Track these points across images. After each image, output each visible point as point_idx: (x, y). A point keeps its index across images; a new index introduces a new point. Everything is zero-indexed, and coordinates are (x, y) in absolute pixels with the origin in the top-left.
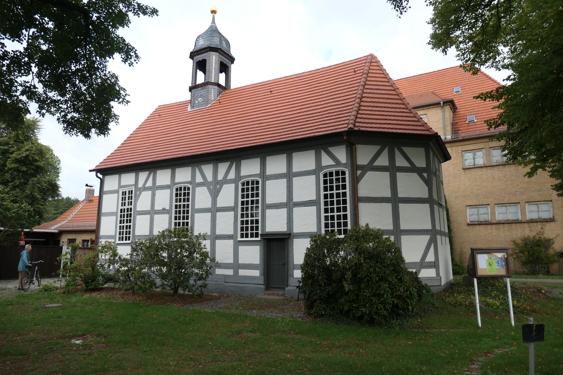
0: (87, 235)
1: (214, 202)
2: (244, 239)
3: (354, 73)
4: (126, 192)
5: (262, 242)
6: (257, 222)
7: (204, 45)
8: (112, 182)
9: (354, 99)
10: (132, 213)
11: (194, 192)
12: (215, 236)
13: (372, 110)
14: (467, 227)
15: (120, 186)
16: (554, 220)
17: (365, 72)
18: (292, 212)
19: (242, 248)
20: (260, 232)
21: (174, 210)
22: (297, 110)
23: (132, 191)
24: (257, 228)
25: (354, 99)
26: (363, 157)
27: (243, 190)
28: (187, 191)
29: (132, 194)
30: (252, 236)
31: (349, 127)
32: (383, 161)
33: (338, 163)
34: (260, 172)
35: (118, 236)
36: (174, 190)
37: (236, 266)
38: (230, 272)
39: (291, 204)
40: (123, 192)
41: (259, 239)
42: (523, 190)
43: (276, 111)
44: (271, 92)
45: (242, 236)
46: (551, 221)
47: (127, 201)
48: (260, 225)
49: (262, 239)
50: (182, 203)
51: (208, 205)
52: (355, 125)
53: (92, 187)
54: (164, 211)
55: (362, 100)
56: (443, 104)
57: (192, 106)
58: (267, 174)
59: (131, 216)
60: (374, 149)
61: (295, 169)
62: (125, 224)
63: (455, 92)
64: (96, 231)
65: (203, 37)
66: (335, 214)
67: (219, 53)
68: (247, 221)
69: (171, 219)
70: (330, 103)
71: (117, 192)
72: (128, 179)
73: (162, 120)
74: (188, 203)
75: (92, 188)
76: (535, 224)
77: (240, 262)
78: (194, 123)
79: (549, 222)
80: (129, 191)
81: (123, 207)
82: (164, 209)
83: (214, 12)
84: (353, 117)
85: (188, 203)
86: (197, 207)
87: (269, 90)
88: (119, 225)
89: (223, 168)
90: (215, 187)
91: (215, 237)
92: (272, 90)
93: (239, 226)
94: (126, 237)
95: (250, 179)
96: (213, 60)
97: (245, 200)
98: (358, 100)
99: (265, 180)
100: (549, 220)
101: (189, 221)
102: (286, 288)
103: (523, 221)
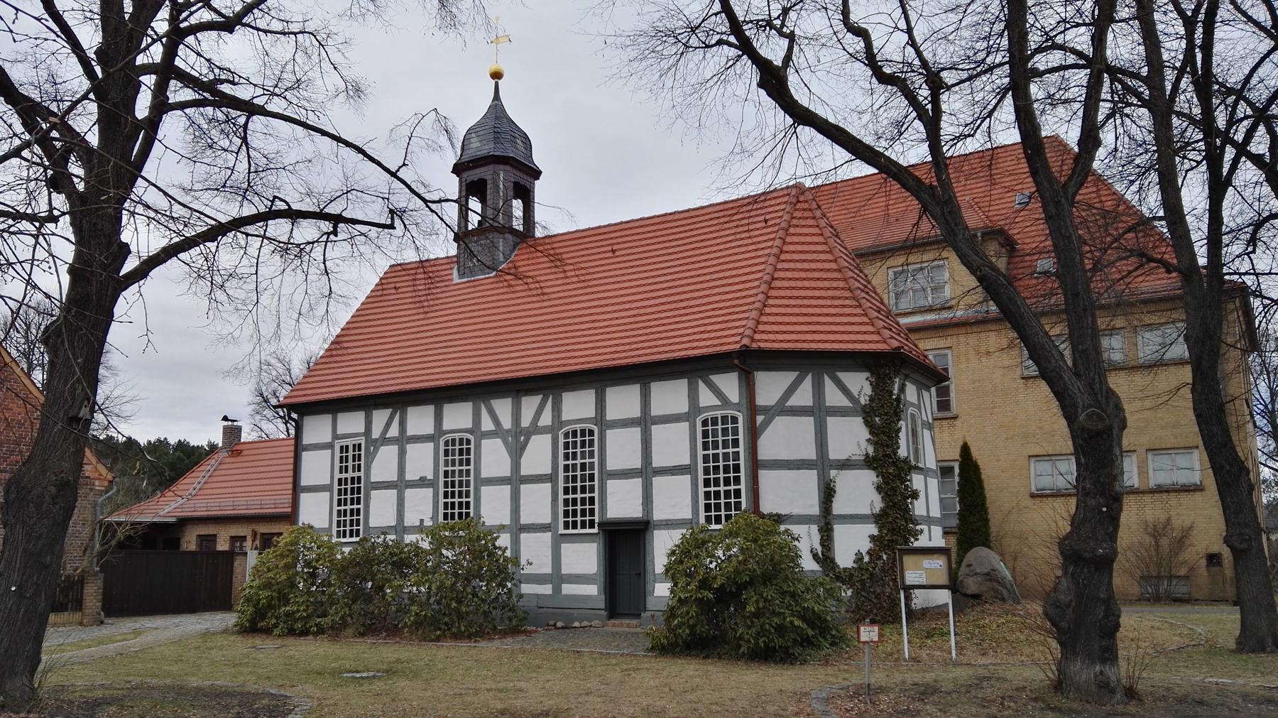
0: (240, 526)
1: (516, 466)
2: (571, 531)
3: (764, 224)
4: (347, 447)
5: (601, 535)
6: (592, 500)
7: (480, 149)
8: (317, 429)
9: (757, 283)
10: (362, 485)
11: (478, 447)
12: (519, 527)
13: (787, 306)
14: (1029, 502)
15: (336, 436)
16: (1202, 487)
17: (783, 225)
18: (651, 484)
19: (566, 548)
20: (597, 519)
21: (442, 480)
22: (679, 246)
23: (360, 445)
24: (592, 512)
25: (757, 283)
26: (770, 386)
27: (566, 446)
28: (465, 447)
29: (360, 450)
30: (583, 526)
31: (743, 343)
32: (803, 396)
33: (725, 402)
34: (596, 414)
35: (335, 529)
37: (557, 578)
38: (547, 589)
40: (342, 447)
41: (595, 530)
42: (1143, 424)
43: (622, 296)
44: (613, 251)
45: (566, 526)
46: (1195, 490)
47: (350, 464)
48: (596, 507)
49: (601, 532)
50: (457, 468)
51: (506, 471)
52: (753, 340)
53: (236, 421)
54: (422, 483)
55: (773, 285)
56: (982, 237)
57: (462, 272)
58: (608, 418)
59: (359, 492)
60: (788, 377)
61: (656, 410)
62: (349, 507)
63: (1019, 204)
64: (291, 517)
65: (479, 133)
66: (722, 488)
67: (512, 166)
68: (575, 501)
69: (438, 496)
70: (717, 287)
71: (330, 446)
72: (352, 423)
73: (402, 299)
74: (468, 468)
75: (235, 423)
76: (1165, 496)
77: (563, 572)
78: (470, 311)
79: (1191, 491)
80: (354, 445)
81: (344, 476)
82: (422, 479)
84: (751, 324)
85: (468, 468)
86: (484, 474)
87: (610, 248)
88: (336, 508)
89: (530, 404)
91: (518, 528)
92: (615, 247)
93: (561, 509)
94: (351, 531)
95: (578, 427)
96: (502, 178)
97: (570, 462)
98: (764, 287)
99: (604, 428)
100: (1191, 488)
101: (471, 500)
102: (643, 614)
103: (1142, 489)
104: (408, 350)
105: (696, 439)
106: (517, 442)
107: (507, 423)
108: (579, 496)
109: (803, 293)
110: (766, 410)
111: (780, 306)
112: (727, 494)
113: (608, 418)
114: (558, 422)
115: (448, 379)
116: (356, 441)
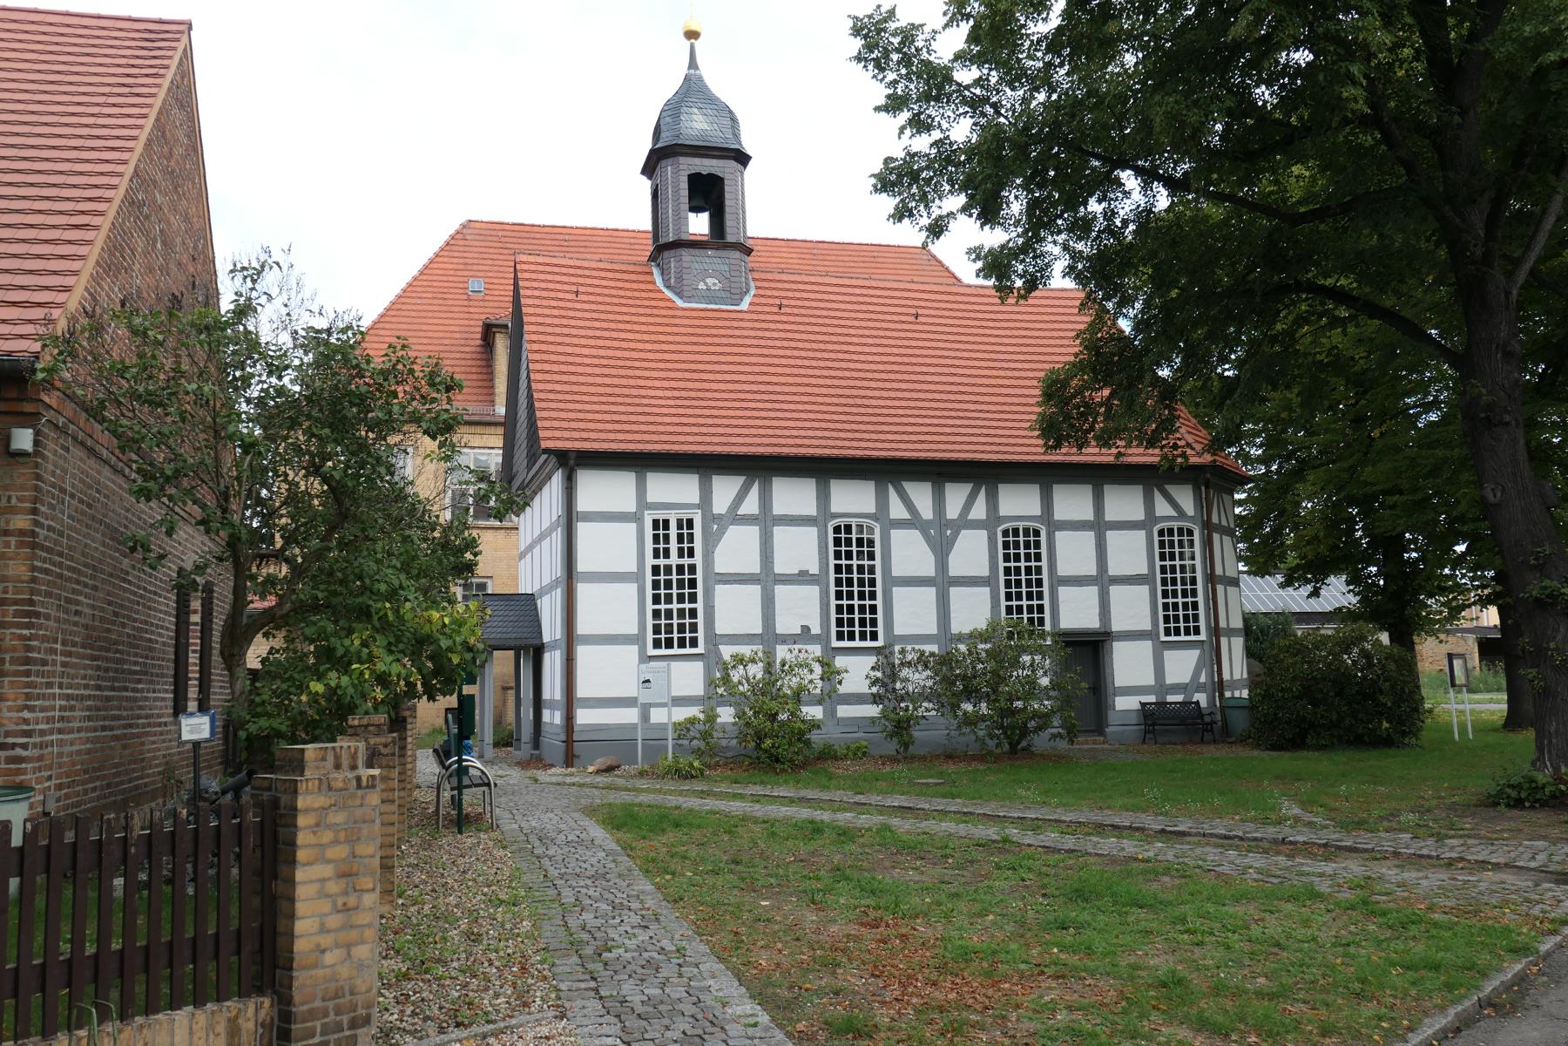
1: (942, 564)
3: (776, 310)
6: (1041, 609)
12: (949, 637)
18: (1108, 593)
19: (1170, 656)
33: (1181, 514)
36: (831, 531)
39: (1106, 579)
45: (840, 636)
54: (803, 578)
58: (1057, 517)
61: (778, 509)
66: (1025, 603)
82: (803, 573)
83: (692, 35)
89: (956, 496)
90: (941, 533)
95: (1021, 525)
104: (789, 398)
105: (827, 548)
106: (941, 538)
107: (927, 512)
108: (675, 606)
109: (824, 391)
110: (718, 518)
111: (716, 391)
112: (681, 613)
113: (1057, 517)
114: (993, 518)
115: (674, 443)
116: (685, 515)
